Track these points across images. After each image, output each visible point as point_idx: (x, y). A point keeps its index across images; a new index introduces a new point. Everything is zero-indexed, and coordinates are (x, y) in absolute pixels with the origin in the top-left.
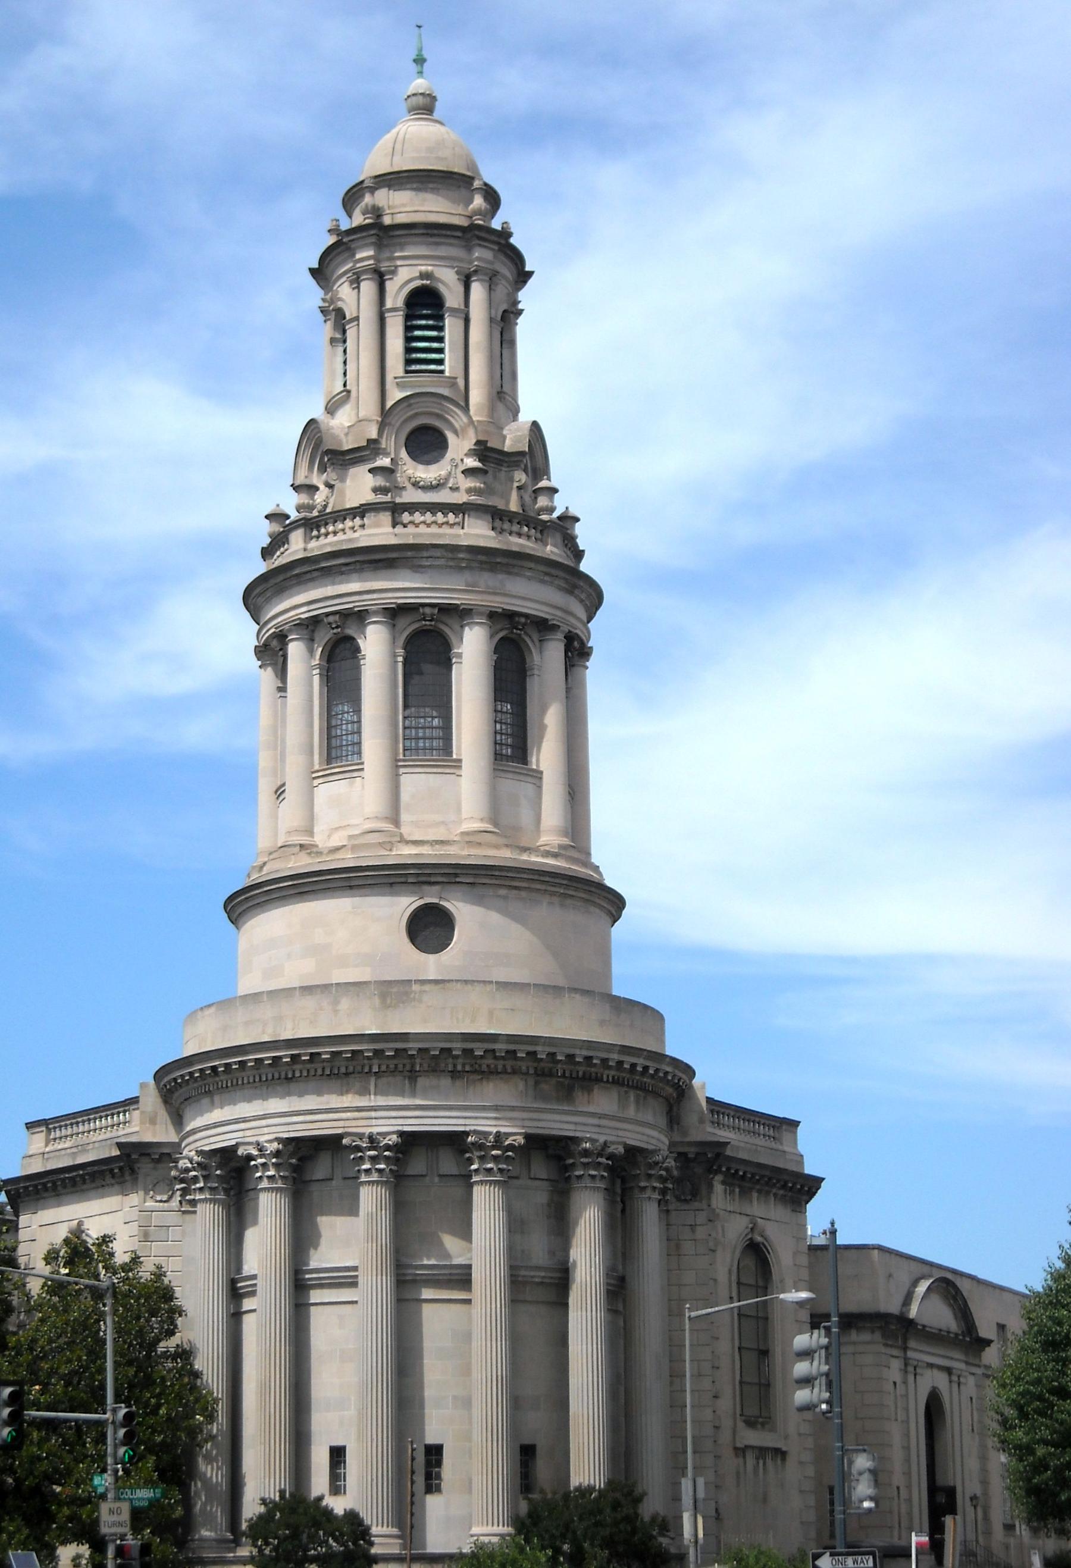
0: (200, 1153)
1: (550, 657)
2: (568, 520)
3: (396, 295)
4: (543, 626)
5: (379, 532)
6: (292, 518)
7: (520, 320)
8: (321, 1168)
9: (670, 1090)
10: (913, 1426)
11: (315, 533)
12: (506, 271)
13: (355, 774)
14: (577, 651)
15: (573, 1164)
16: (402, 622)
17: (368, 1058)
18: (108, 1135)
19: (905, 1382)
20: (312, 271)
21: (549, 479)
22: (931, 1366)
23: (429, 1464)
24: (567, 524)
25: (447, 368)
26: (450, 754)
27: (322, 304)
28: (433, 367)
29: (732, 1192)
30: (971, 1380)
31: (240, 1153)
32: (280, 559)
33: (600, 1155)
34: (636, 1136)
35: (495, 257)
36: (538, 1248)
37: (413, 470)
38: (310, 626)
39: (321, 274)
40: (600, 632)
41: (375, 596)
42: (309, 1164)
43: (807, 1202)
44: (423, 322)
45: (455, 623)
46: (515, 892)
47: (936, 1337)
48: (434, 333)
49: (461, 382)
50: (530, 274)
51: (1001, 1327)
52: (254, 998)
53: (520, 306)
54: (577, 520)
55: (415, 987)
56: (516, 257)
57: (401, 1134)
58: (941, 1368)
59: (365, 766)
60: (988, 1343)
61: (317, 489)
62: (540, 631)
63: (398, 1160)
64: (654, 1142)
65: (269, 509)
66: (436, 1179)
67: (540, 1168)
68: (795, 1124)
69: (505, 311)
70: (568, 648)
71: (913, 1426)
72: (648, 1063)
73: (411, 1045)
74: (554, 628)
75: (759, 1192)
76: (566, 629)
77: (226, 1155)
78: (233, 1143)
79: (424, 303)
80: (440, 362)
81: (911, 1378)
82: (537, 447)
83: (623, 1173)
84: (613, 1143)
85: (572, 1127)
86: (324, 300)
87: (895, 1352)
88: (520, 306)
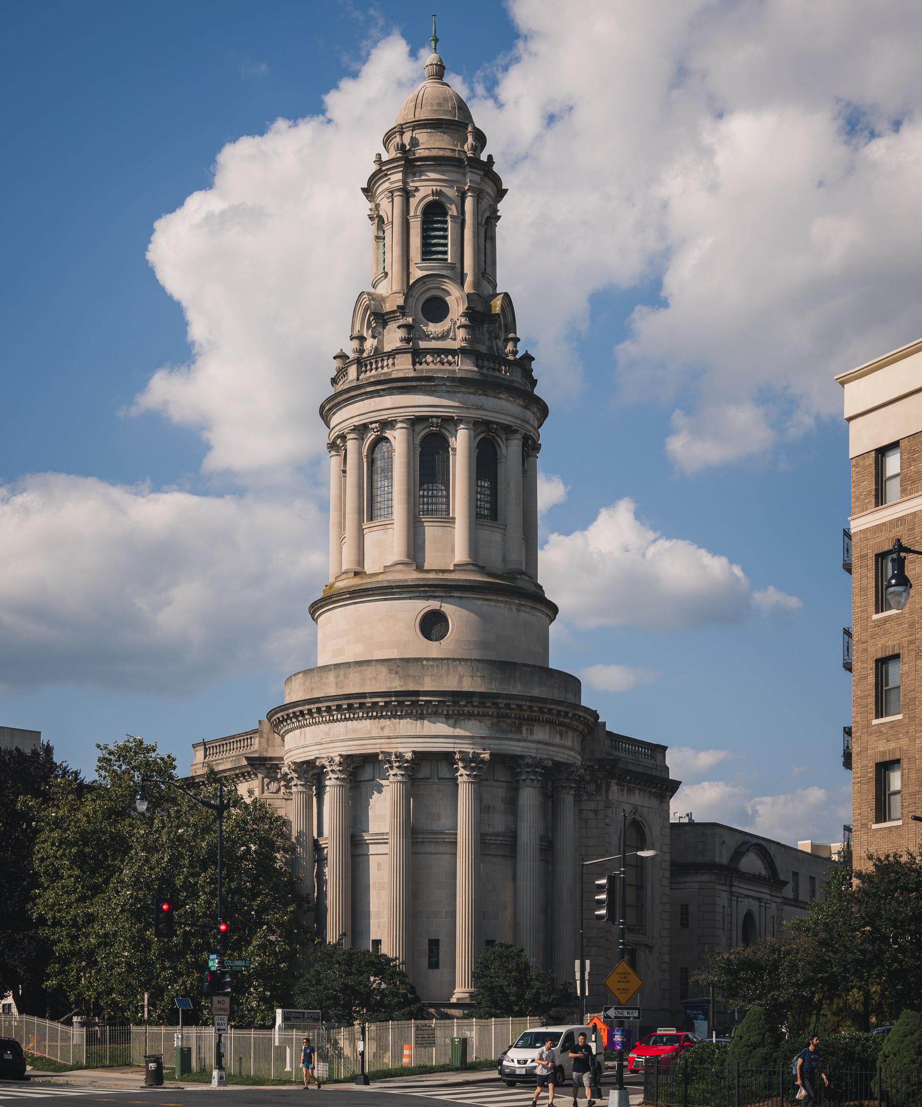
0: (295, 763)
1: (511, 450)
2: (528, 358)
3: (416, 205)
4: (509, 430)
5: (403, 366)
6: (351, 359)
7: (499, 223)
8: (367, 773)
9: (581, 727)
10: (734, 933)
11: (364, 369)
12: (490, 189)
13: (389, 526)
14: (531, 447)
15: (520, 772)
16: (418, 428)
17: (449, 706)
18: (241, 752)
19: (730, 906)
20: (364, 190)
21: (515, 333)
22: (748, 897)
23: (431, 950)
24: (525, 362)
25: (449, 257)
26: (449, 514)
27: (370, 213)
28: (440, 256)
29: (622, 790)
30: (774, 905)
31: (317, 764)
32: (341, 387)
33: (537, 767)
34: (562, 756)
35: (482, 179)
36: (499, 823)
37: (433, 328)
38: (361, 430)
39: (368, 192)
40: (546, 434)
41: (402, 410)
42: (360, 770)
43: (671, 797)
44: (439, 226)
45: (451, 427)
46: (487, 602)
47: (754, 879)
48: (441, 233)
49: (458, 266)
50: (506, 190)
51: (796, 874)
52: (326, 668)
53: (499, 214)
54: (533, 359)
55: (425, 662)
56: (496, 180)
57: (414, 752)
58: (753, 898)
59: (394, 522)
60: (785, 883)
61: (365, 339)
62: (506, 434)
63: (413, 768)
64: (572, 759)
65: (336, 352)
66: (437, 781)
67: (502, 775)
68: (665, 748)
69: (488, 217)
70: (525, 444)
71: (734, 933)
72: (568, 710)
73: (421, 698)
74: (516, 431)
75: (640, 790)
76: (523, 432)
77: (310, 764)
78: (313, 757)
79: (434, 212)
80: (445, 253)
81: (734, 903)
82: (508, 310)
83: (552, 777)
84: (545, 759)
85: (452, 745)
86: (371, 210)
87: (724, 888)
88: (499, 214)
